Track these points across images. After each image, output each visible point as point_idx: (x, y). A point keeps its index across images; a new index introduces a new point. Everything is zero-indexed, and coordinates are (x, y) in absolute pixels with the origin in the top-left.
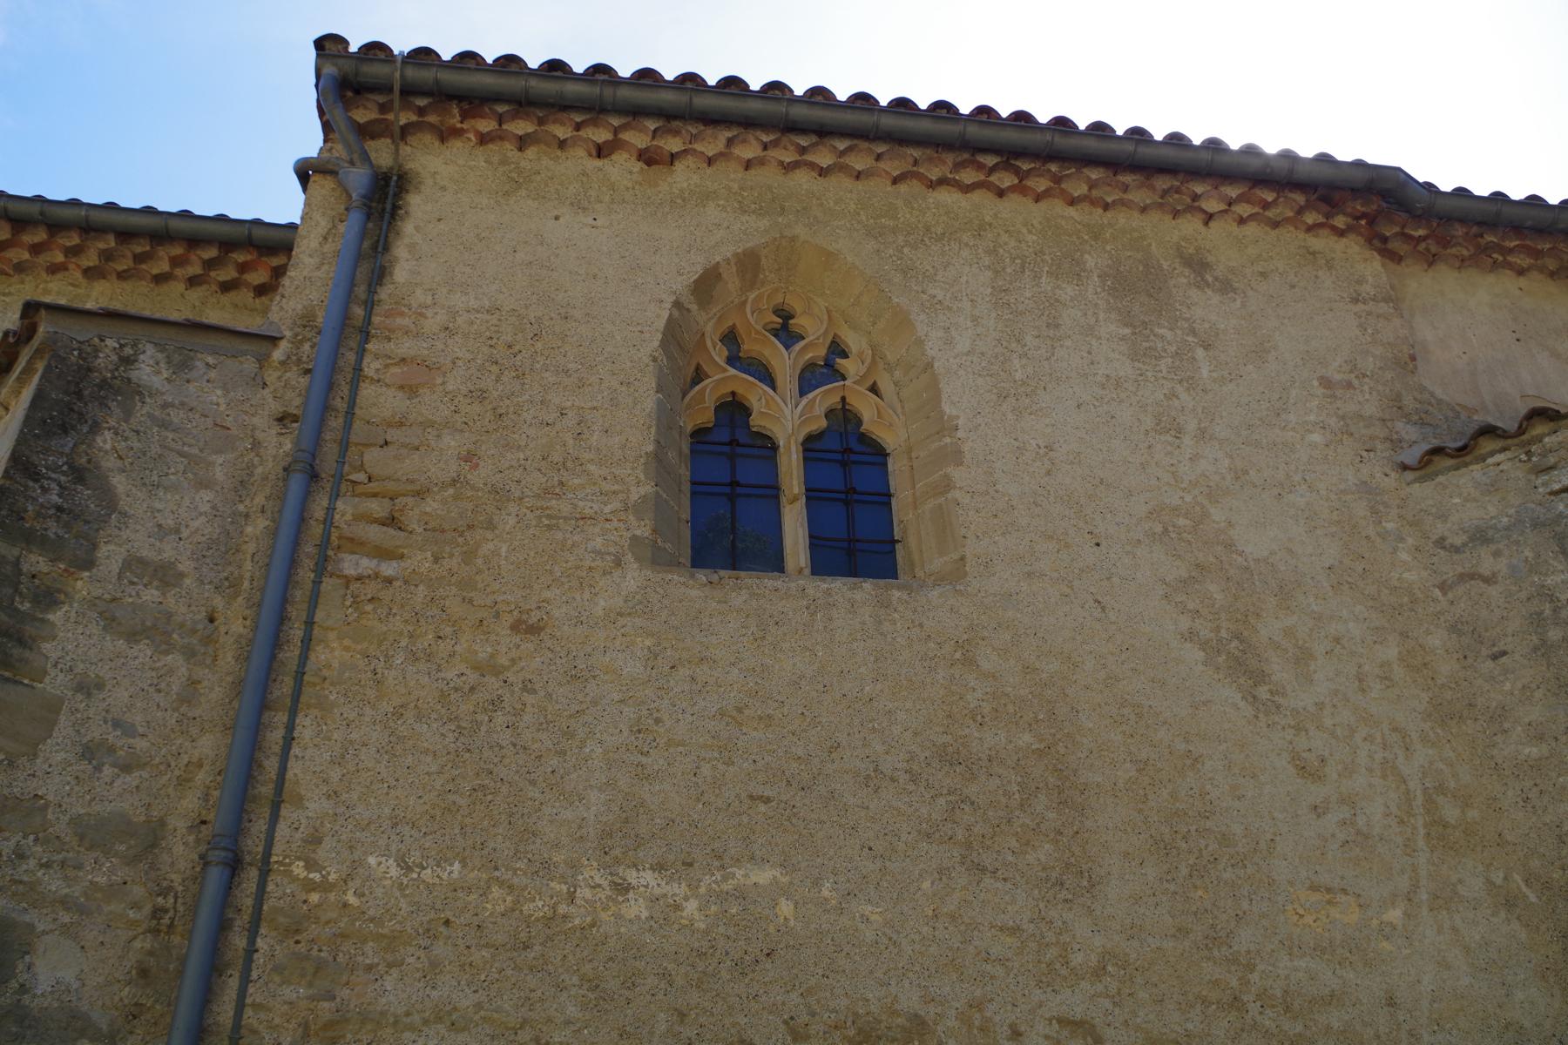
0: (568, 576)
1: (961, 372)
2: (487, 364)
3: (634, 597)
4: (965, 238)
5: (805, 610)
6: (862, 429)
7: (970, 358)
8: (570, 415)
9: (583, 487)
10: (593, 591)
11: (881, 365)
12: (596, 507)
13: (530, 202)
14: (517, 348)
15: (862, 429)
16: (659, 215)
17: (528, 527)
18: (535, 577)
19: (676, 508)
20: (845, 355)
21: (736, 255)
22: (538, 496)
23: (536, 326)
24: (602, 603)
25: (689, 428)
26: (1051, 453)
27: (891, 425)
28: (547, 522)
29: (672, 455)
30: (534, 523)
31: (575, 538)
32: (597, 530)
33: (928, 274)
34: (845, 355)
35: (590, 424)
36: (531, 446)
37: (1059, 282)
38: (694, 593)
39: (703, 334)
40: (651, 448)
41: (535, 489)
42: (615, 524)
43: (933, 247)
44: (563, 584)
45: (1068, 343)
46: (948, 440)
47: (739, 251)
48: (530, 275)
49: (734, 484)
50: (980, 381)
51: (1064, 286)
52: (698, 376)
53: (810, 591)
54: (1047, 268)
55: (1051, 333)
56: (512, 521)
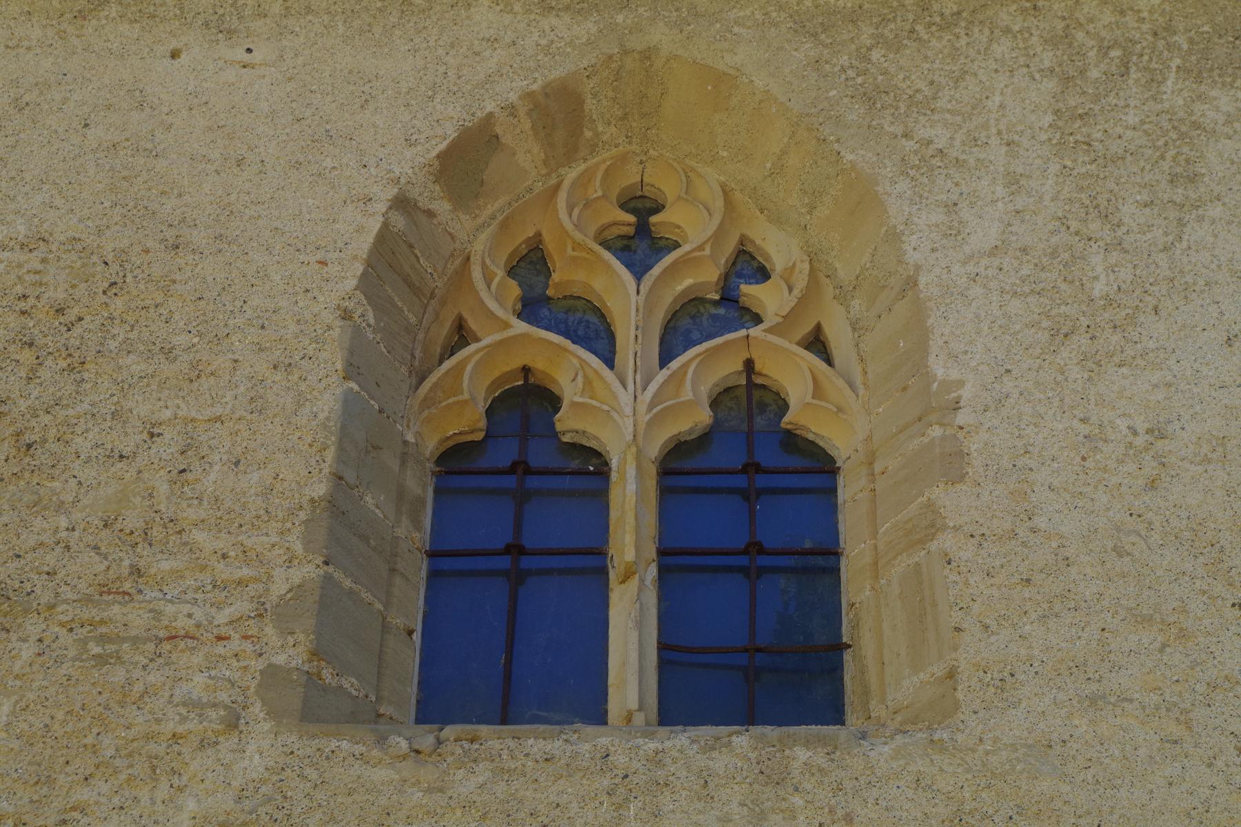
0: (130, 755)
1: (977, 290)
2: (12, 348)
3: (257, 790)
4: (1004, 18)
5: (605, 798)
6: (788, 420)
7: (996, 262)
8: (167, 436)
9: (179, 575)
10: (176, 782)
11: (829, 291)
12: (199, 614)
13: (124, 28)
14: (72, 314)
15: (788, 420)
16: (377, 30)
17: (59, 662)
18: (62, 760)
19: (379, 606)
20: (762, 274)
21: (528, 96)
22: (87, 600)
23: (115, 268)
24: (191, 805)
25: (431, 446)
26: (1160, 443)
27: (840, 410)
28: (96, 650)
29: (372, 502)
30: (72, 653)
31: (151, 678)
32: (198, 659)
33: (919, 97)
34: (762, 274)
35: (204, 451)
36: (85, 501)
37: (1203, 87)
38: (381, 774)
39: (468, 259)
40: (320, 489)
41: (82, 586)
42: (235, 644)
43: (934, 42)
44: (116, 771)
45: (1215, 211)
46: (936, 432)
47: (535, 87)
48: (112, 169)
49: (515, 550)
50: (1015, 306)
51: (1213, 93)
52: (461, 336)
53: (620, 759)
54: (1178, 61)
55: (1179, 194)
56: (27, 652)
